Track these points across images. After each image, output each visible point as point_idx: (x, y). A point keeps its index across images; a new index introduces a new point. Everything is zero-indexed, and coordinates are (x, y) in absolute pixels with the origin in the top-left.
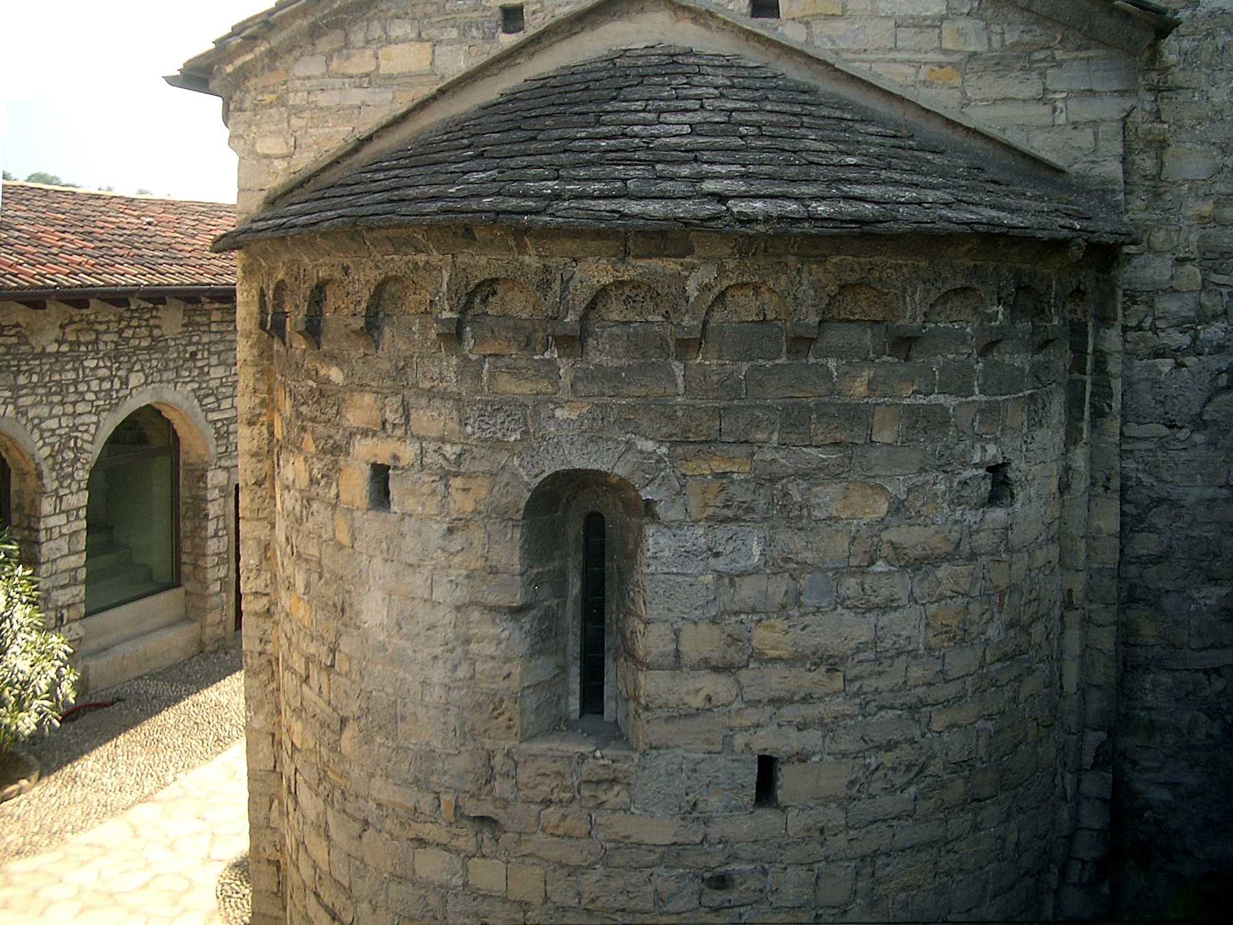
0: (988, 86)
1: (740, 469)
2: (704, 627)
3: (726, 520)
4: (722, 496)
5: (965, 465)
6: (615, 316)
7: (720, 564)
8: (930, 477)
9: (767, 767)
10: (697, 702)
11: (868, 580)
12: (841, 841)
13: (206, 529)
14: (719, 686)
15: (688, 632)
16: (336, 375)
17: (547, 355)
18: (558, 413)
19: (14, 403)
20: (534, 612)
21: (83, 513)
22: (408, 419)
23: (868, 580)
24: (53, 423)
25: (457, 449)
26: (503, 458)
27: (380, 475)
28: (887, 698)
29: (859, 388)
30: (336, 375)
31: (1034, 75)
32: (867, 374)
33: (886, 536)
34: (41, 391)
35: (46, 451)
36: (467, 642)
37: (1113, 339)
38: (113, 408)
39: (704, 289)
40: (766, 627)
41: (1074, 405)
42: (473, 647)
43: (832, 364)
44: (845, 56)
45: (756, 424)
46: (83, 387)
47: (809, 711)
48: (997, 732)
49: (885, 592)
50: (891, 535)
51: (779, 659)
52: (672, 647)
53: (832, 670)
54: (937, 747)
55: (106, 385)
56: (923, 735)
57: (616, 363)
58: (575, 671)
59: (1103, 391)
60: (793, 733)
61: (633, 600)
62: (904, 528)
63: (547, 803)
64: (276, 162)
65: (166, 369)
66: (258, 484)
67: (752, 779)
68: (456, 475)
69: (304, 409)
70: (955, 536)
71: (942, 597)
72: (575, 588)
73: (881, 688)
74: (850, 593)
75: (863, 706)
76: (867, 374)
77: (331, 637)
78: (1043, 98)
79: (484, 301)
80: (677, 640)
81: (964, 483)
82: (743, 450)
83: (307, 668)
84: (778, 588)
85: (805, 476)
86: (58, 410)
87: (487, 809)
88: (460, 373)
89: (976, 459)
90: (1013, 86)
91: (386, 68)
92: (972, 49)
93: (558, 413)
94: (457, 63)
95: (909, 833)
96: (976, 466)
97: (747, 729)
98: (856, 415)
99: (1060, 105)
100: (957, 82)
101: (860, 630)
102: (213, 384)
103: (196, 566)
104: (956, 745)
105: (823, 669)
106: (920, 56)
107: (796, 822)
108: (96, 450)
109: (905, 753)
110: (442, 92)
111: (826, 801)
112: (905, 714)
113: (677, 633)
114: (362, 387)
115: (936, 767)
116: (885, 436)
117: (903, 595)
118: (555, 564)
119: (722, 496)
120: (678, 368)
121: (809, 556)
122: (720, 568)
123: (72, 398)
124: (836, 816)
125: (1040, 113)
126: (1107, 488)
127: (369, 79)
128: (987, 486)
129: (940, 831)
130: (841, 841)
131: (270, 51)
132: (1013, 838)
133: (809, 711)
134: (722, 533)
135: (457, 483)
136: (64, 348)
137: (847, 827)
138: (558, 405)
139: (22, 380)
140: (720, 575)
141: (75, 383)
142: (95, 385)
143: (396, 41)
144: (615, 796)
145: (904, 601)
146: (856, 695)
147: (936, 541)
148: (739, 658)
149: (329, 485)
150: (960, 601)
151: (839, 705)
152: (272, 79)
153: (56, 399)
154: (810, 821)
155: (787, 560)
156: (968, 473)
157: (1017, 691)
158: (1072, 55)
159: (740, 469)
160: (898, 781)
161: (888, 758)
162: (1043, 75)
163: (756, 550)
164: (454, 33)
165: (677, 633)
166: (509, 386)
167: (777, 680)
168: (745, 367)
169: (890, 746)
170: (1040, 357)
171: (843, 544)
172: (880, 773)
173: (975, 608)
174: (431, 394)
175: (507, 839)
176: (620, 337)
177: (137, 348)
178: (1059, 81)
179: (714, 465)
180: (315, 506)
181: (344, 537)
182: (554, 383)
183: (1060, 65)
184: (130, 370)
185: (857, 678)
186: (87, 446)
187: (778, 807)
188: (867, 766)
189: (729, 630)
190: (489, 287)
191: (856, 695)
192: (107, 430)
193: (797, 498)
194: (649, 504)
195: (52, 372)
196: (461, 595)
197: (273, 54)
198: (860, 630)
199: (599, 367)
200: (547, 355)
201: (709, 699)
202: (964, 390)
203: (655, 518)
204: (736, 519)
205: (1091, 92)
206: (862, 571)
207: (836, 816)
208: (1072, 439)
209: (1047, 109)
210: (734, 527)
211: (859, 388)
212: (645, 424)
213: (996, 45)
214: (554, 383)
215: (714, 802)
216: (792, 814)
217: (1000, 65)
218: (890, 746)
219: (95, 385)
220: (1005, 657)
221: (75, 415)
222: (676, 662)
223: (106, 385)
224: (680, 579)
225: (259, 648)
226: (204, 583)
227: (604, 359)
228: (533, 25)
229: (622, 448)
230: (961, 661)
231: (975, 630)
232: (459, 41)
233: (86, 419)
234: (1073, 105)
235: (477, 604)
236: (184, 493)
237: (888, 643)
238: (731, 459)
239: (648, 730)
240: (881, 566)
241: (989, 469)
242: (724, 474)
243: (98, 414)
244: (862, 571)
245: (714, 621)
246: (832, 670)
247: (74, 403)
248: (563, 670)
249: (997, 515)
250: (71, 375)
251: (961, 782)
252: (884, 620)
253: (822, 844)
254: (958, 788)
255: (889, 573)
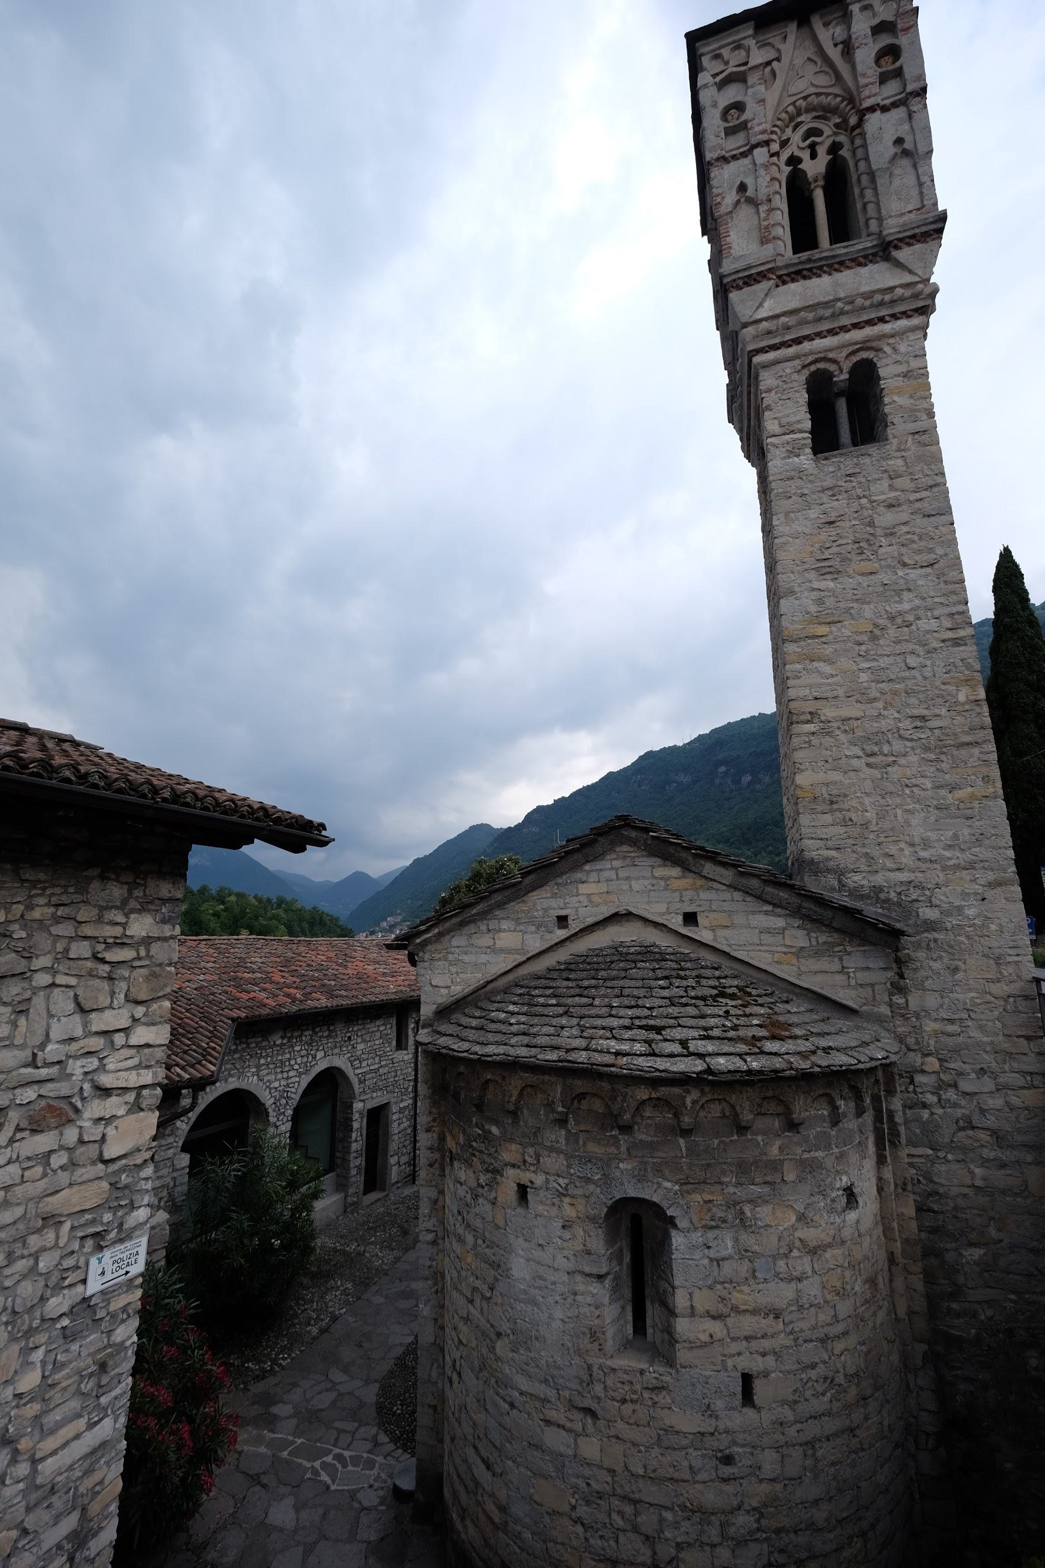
0: (812, 964)
1: (718, 1199)
2: (705, 1291)
3: (712, 1228)
4: (710, 1214)
5: (832, 1189)
6: (648, 1114)
7: (712, 1254)
8: (815, 1199)
9: (747, 1380)
10: (704, 1338)
11: (790, 1262)
12: (792, 1431)
13: (351, 1137)
14: (717, 1328)
15: (697, 1295)
16: (495, 1130)
17: (613, 1133)
18: (621, 1165)
19: (258, 1075)
20: (610, 1277)
21: (288, 1135)
22: (538, 1161)
23: (790, 1262)
24: (276, 1084)
25: (566, 1181)
26: (591, 1187)
27: (523, 1191)
28: (808, 1334)
29: (774, 1151)
30: (495, 1130)
31: (836, 960)
32: (778, 1143)
33: (797, 1234)
34: (271, 1066)
35: (272, 1100)
36: (575, 1294)
37: (897, 1104)
38: (307, 1072)
39: (694, 1102)
40: (738, 1291)
41: (880, 1143)
42: (579, 1298)
43: (760, 1138)
44: (734, 947)
45: (724, 1172)
46: (293, 1062)
47: (766, 1344)
48: (869, 1352)
49: (799, 1268)
50: (797, 1234)
51: (747, 1311)
52: (688, 1303)
53: (777, 1317)
54: (839, 1365)
55: (305, 1059)
56: (830, 1358)
57: (649, 1139)
58: (629, 1308)
59: (895, 1133)
60: (759, 1358)
61: (664, 1272)
62: (805, 1229)
63: (624, 1401)
64: (442, 990)
65: (335, 1047)
66: (431, 1165)
67: (739, 1389)
68: (565, 1196)
69: (474, 1144)
70: (832, 1232)
71: (830, 1269)
72: (627, 1259)
73: (805, 1328)
74: (781, 1270)
75: (796, 1340)
76: (778, 1143)
77: (490, 1280)
78: (843, 970)
79: (579, 1102)
80: (691, 1299)
81: (833, 1201)
82: (719, 1187)
83: (473, 1295)
84: (744, 1268)
85: (750, 1201)
86: (280, 1076)
87: (588, 1403)
88: (567, 1139)
89: (838, 1186)
90: (824, 964)
91: (499, 944)
92: (802, 945)
93: (621, 1165)
94: (535, 944)
95: (830, 1425)
96: (838, 1189)
97: (733, 1356)
98: (775, 1166)
99: (852, 975)
100: (795, 961)
101: (788, 1292)
102: (359, 1053)
103: (344, 1159)
104: (851, 1363)
105: (771, 1316)
106: (774, 949)
107: (767, 1417)
108: (297, 1097)
109: (821, 1370)
110: (528, 959)
111: (783, 1402)
112: (819, 1345)
113: (691, 1294)
114: (512, 1140)
115: (840, 1379)
116: (790, 1177)
117: (809, 1270)
118: (619, 1244)
119: (710, 1214)
120: (682, 1141)
121: (756, 1248)
122: (712, 1256)
123: (287, 1069)
124: (788, 1414)
125: (840, 979)
126: (904, 1190)
127: (493, 950)
128: (844, 1200)
129: (848, 1422)
130: (792, 1431)
131: (439, 932)
132: (886, 1423)
133: (766, 1344)
134: (711, 1234)
135: (567, 1200)
136: (285, 1041)
137: (796, 1422)
138: (621, 1160)
139: (262, 1061)
140: (711, 1260)
141: (289, 1060)
142: (299, 1060)
143: (504, 931)
144: (663, 1398)
145: (810, 1273)
146: (791, 1333)
147: (823, 1236)
148: (726, 1311)
149: (490, 1191)
150: (839, 1270)
151: (783, 1340)
152: (439, 946)
153: (279, 1070)
154: (774, 1418)
155: (746, 1251)
156: (834, 1195)
157: (875, 1323)
158: (855, 949)
159: (718, 1199)
160: (820, 1388)
161: (813, 1374)
162: (841, 959)
163: (730, 1244)
164: (533, 928)
165: (691, 1294)
166: (593, 1148)
167: (748, 1324)
168: (716, 1142)
169: (813, 1366)
170: (860, 1120)
171: (774, 1240)
172: (809, 1384)
173: (848, 1274)
174: (551, 1149)
175: (601, 1423)
176: (651, 1125)
177: (322, 1037)
178: (851, 962)
179: (704, 1195)
180: (481, 1200)
181: (501, 1223)
182: (618, 1148)
183: (849, 954)
184: (318, 1050)
185: (791, 1322)
186: (293, 1096)
187: (754, 1406)
188: (801, 1380)
189: (718, 1293)
190: (582, 1096)
191: (791, 1333)
192: (304, 1084)
193: (748, 1214)
194: (672, 1218)
195: (278, 1054)
196: (570, 1266)
197: (440, 935)
198: (788, 1292)
199: (641, 1141)
200: (613, 1133)
201: (711, 1336)
202: (828, 1147)
203: (675, 1226)
204: (717, 1227)
205: (868, 968)
206: (786, 1256)
207: (788, 1414)
208: (881, 1160)
209: (844, 977)
210: (717, 1232)
211: (774, 1151)
212: (667, 1172)
213: (814, 943)
214: (618, 1148)
215: (719, 1405)
216: (763, 1413)
217: (818, 954)
218: (813, 1366)
219: (299, 1060)
220: (866, 1302)
221: (288, 1078)
222: (692, 1312)
223: (305, 1059)
224: (690, 1262)
225: (428, 1263)
226: (348, 1169)
227: (643, 1137)
228: (574, 926)
229: (655, 1186)
230: (845, 1308)
231: (848, 1287)
232: (535, 933)
233: (293, 1080)
234: (859, 975)
235: (579, 1272)
236: (339, 1116)
237: (805, 1300)
238: (712, 1193)
239: (683, 1355)
240: (795, 1253)
241: (844, 1190)
242: (710, 1201)
243: (299, 1076)
244: (786, 1256)
245: (710, 1288)
246: (777, 1317)
247: (288, 1072)
248: (623, 1308)
249: (852, 1216)
250: (288, 1056)
251: (854, 1387)
252: (800, 1286)
253: (783, 1434)
254: (853, 1391)
255: (800, 1257)
